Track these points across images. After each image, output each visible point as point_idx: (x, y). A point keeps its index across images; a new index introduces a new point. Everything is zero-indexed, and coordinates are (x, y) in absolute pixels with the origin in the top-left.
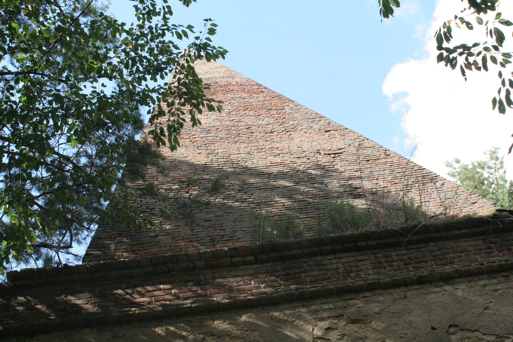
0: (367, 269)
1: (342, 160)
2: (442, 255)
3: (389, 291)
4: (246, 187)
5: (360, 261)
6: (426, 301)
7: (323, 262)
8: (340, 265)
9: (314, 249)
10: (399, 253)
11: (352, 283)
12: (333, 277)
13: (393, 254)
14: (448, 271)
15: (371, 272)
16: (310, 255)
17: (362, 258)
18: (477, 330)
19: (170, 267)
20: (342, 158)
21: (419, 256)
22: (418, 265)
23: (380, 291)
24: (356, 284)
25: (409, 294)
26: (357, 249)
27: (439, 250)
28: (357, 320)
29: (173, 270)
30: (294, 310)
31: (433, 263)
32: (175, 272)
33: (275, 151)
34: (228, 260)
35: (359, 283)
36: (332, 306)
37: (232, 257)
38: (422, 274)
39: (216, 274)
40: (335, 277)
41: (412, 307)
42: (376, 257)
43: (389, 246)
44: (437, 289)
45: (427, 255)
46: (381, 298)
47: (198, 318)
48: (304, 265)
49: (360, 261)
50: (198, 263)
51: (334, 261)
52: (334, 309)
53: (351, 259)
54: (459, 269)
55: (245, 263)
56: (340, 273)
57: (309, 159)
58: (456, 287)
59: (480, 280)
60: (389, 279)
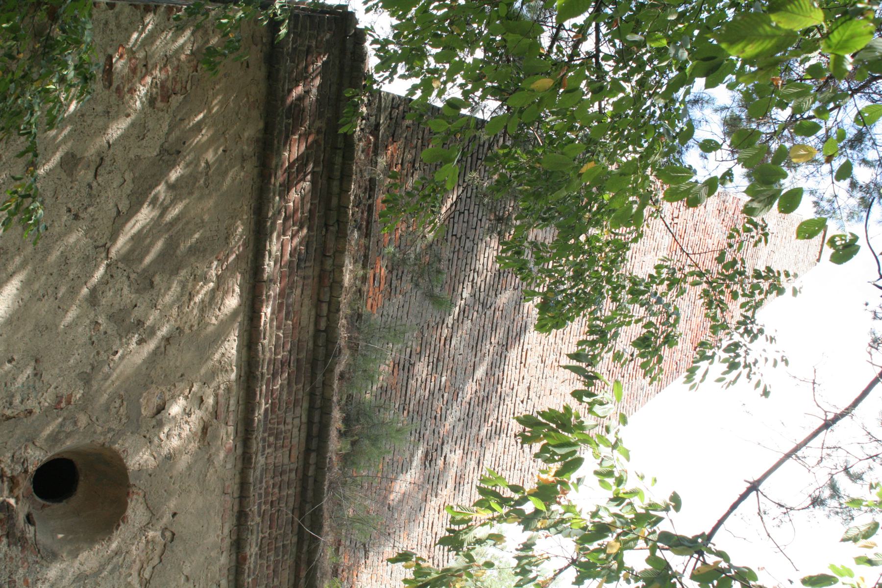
0: (275, 457)
1: (507, 446)
2: (276, 548)
3: (238, 476)
4: (488, 313)
5: (290, 451)
6: (213, 514)
7: (299, 408)
8: (290, 427)
9: (319, 402)
10: (291, 500)
11: (256, 438)
12: (274, 416)
13: (291, 492)
14: (247, 549)
15: (271, 460)
16: (312, 394)
17: (295, 453)
18: (161, 561)
19: (331, 228)
20: (511, 447)
21: (280, 521)
22: (267, 517)
23: (239, 466)
24: (254, 442)
25: (228, 498)
26: (308, 451)
27: (284, 546)
28: (206, 433)
29: (327, 230)
30: (236, 366)
31: (267, 535)
32: (324, 233)
33: (553, 357)
34: (326, 298)
35: (255, 445)
36: (232, 408)
37: (330, 303)
38: (250, 519)
39: (310, 281)
40: (272, 419)
41: (209, 498)
42: (291, 471)
43: (304, 489)
44: (226, 531)
45: (280, 529)
46: (229, 466)
47: (250, 256)
48: (300, 386)
49: (290, 451)
50: (329, 262)
51: (297, 421)
52: (228, 411)
53: (295, 441)
54: (247, 562)
55: (318, 317)
56: (278, 424)
57: (522, 402)
58: (224, 553)
59: (229, 582)
60: (251, 480)
